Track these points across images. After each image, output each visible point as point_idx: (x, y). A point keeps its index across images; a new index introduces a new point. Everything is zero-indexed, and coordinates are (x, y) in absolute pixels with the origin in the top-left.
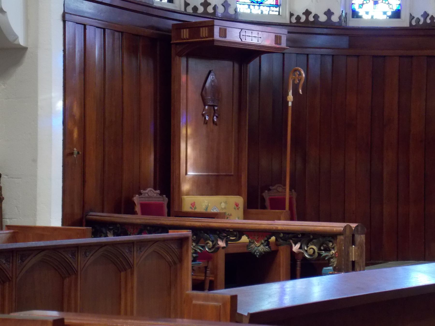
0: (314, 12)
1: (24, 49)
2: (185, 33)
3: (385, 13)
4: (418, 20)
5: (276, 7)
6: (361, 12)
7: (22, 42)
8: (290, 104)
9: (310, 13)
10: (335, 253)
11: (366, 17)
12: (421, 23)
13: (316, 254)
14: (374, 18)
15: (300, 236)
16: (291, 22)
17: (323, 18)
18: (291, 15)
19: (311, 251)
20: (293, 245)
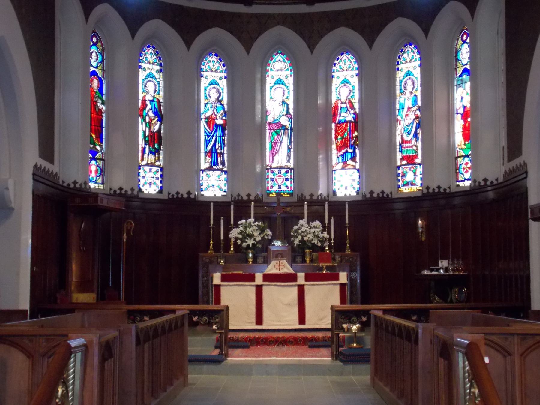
0: (181, 192)
1: (12, 209)
2: (78, 200)
3: (155, 190)
4: (173, 196)
5: (102, 185)
6: (143, 189)
7: (13, 205)
8: (125, 240)
9: (179, 193)
10: (219, 321)
11: (146, 192)
12: (237, 199)
13: (207, 321)
14: (150, 193)
15: (205, 313)
16: (232, 200)
17: (186, 196)
18: (111, 189)
19: (205, 320)
20: (194, 318)
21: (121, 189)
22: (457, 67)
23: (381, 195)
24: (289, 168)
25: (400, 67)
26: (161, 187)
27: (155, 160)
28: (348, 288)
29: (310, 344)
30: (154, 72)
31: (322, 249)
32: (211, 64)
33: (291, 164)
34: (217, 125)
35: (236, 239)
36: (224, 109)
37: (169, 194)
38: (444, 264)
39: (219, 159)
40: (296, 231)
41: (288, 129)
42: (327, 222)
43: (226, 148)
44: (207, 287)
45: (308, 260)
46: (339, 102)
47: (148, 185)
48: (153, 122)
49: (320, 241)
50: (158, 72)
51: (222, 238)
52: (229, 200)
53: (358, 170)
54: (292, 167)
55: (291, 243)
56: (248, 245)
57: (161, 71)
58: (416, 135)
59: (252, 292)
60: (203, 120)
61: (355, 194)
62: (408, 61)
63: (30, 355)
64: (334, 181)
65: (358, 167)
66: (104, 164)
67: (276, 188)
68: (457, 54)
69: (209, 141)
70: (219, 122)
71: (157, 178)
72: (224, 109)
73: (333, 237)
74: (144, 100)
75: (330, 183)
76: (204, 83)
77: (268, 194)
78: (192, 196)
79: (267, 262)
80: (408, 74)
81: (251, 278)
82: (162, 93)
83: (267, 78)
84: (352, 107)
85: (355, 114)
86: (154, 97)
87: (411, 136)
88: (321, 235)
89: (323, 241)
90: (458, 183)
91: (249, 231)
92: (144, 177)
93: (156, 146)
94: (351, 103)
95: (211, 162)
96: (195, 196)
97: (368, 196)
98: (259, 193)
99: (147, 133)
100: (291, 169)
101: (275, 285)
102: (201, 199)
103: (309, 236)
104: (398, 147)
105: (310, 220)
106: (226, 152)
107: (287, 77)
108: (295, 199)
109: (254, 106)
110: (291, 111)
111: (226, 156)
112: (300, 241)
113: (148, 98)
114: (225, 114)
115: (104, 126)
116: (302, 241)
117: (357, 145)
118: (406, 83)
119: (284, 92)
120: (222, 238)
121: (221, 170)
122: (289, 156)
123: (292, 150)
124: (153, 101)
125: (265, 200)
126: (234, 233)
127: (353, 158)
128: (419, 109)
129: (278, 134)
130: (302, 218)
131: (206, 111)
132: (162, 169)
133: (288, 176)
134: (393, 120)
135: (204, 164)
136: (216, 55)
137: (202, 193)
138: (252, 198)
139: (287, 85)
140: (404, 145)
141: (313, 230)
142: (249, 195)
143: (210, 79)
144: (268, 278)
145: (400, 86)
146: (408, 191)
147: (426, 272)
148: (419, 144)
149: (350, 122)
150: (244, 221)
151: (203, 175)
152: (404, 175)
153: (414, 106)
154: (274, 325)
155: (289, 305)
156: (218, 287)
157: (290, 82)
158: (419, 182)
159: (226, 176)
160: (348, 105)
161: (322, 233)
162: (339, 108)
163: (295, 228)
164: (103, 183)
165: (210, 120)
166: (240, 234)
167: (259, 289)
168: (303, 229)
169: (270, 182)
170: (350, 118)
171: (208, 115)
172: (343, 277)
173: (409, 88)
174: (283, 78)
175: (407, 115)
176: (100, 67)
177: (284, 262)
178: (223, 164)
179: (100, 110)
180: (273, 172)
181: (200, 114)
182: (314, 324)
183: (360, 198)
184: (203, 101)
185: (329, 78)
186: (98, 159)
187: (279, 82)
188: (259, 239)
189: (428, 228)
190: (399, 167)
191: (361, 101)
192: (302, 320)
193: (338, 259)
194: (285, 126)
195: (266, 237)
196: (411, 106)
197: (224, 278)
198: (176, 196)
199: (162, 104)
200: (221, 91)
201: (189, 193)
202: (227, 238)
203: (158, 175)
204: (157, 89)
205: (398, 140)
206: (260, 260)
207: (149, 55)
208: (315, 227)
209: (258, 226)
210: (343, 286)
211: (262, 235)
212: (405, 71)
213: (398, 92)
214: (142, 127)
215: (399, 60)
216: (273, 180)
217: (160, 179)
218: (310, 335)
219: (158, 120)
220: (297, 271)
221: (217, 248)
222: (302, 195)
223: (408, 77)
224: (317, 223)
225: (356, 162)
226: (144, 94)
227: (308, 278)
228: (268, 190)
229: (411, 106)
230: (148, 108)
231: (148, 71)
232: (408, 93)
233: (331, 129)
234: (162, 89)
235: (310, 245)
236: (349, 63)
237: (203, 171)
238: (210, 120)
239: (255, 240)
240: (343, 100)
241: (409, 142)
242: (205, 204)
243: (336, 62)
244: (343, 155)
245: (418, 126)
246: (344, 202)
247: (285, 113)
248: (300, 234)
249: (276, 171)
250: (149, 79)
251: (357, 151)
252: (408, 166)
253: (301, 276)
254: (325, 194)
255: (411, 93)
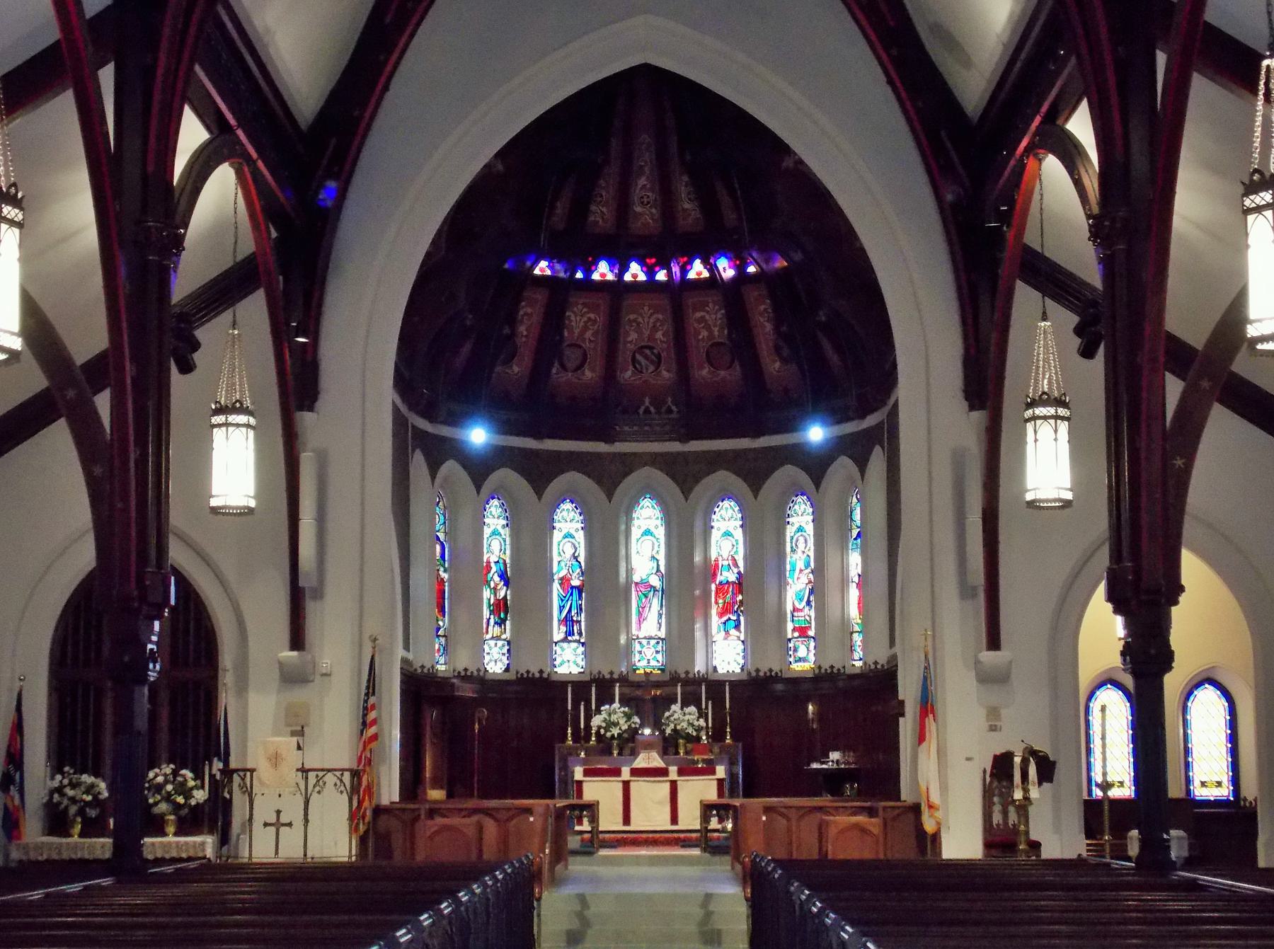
4: (522, 674)
11: (491, 671)
17: (537, 675)
21: (466, 670)
22: (851, 530)
23: (768, 674)
24: (659, 638)
25: (790, 520)
26: (508, 664)
27: (501, 632)
28: (726, 785)
29: (681, 844)
30: (499, 528)
31: (698, 739)
32: (565, 513)
33: (662, 634)
34: (573, 587)
35: (600, 727)
36: (581, 567)
37: (517, 673)
38: (835, 756)
39: (575, 628)
40: (668, 718)
41: (658, 591)
42: (704, 706)
43: (583, 615)
44: (566, 783)
45: (682, 752)
46: (720, 559)
47: (493, 663)
48: (499, 588)
49: (696, 730)
50: (503, 527)
51: (582, 726)
52: (587, 678)
53: (743, 642)
54: (663, 637)
55: (663, 732)
56: (613, 736)
57: (507, 525)
58: (808, 603)
59: (619, 788)
60: (556, 581)
61: (739, 671)
62: (800, 514)
63: (496, 820)
64: (714, 655)
65: (742, 638)
66: (446, 640)
67: (644, 663)
68: (851, 512)
69: (564, 606)
70: (575, 582)
71: (504, 654)
72: (581, 567)
73: (710, 725)
74: (488, 562)
75: (710, 656)
76: (557, 536)
77: (635, 670)
78: (545, 675)
79: (634, 753)
80: (800, 529)
81: (616, 772)
82: (508, 552)
83: (632, 528)
84: (736, 565)
85: (739, 573)
86: (499, 557)
87: (804, 603)
88: (696, 723)
89: (699, 729)
90: (854, 663)
91: (614, 718)
92: (488, 654)
93: (502, 615)
94: (734, 560)
95: (566, 632)
96: (549, 675)
97: (754, 674)
98: (623, 670)
99: (492, 602)
100: (662, 639)
101: (644, 781)
102: (554, 678)
103: (682, 724)
104: (789, 616)
105: (685, 704)
106: (583, 620)
107: (657, 527)
108: (667, 677)
109: (617, 566)
110: (662, 569)
111: (583, 624)
112: (672, 730)
113: (493, 559)
114: (582, 573)
115: (446, 597)
116: (675, 730)
117: (741, 611)
118: (797, 541)
119: (653, 544)
120: (582, 726)
121: (578, 641)
122: (660, 624)
123: (664, 616)
124: (498, 562)
125: (631, 678)
126: (597, 721)
127: (737, 627)
128: (812, 572)
129: (646, 597)
130: (675, 701)
131: (559, 571)
132: (509, 643)
133: (659, 648)
134: (782, 583)
135: (558, 633)
136: (572, 502)
137: (555, 670)
138: (616, 676)
139: (657, 536)
140: (796, 614)
141: (687, 717)
142: (611, 673)
143: (565, 531)
144: (636, 772)
145: (791, 543)
146: (800, 669)
147: (815, 766)
148: (813, 614)
149: (733, 583)
150: (607, 707)
151: (557, 648)
152: (795, 650)
153: (806, 568)
154: (643, 826)
155: (660, 803)
156: (580, 783)
157: (661, 532)
158: (812, 658)
159: (583, 649)
160: (730, 562)
161: (698, 720)
162: (720, 566)
163: (667, 714)
164: (445, 664)
165: (564, 581)
166: (604, 721)
167: (626, 785)
168: (676, 716)
169: (637, 655)
170: (732, 577)
171: (561, 575)
172: (721, 771)
173: (801, 545)
174: (652, 529)
175: (798, 578)
176: (442, 530)
177: (655, 755)
178: (580, 634)
179: (442, 579)
180: (640, 643)
181: (553, 575)
182: (689, 825)
183: (745, 677)
184: (556, 558)
185: (708, 529)
186: (440, 636)
187: (647, 532)
188: (625, 727)
189: (820, 715)
190: (790, 640)
191: (745, 559)
192: (674, 820)
193: (716, 750)
194: (654, 587)
195: (633, 726)
196: (803, 568)
197: (587, 773)
198: (525, 676)
199: (508, 566)
200: (577, 545)
201: (541, 672)
202: (588, 727)
203: (505, 650)
204: (503, 548)
205: (789, 608)
206: (627, 751)
207: (494, 507)
208: (690, 714)
209: (624, 712)
210: (720, 781)
211: (629, 723)
212: (797, 526)
213: (788, 549)
214: (487, 594)
215: (789, 512)
216: (640, 652)
217: (507, 655)
218: (682, 835)
219: (504, 585)
220: (668, 764)
221: (576, 738)
222: (676, 672)
223: (800, 533)
224: (692, 709)
225: (740, 632)
226: (488, 555)
227: (681, 772)
228: (635, 665)
229: (803, 568)
230: (492, 572)
231: (492, 528)
232: (799, 551)
233: (710, 591)
234: (508, 547)
235: (683, 734)
236: (732, 512)
237: (556, 643)
238: (564, 581)
239: (620, 729)
240: (725, 557)
241: (801, 610)
242: (560, 686)
243: (716, 509)
244: (725, 623)
245: (811, 592)
246: (725, 681)
247: (654, 571)
248: (673, 722)
249: (644, 642)
250: (494, 537)
251: (742, 618)
252: (800, 639)
253: (673, 770)
254: (703, 671)
255: (804, 552)
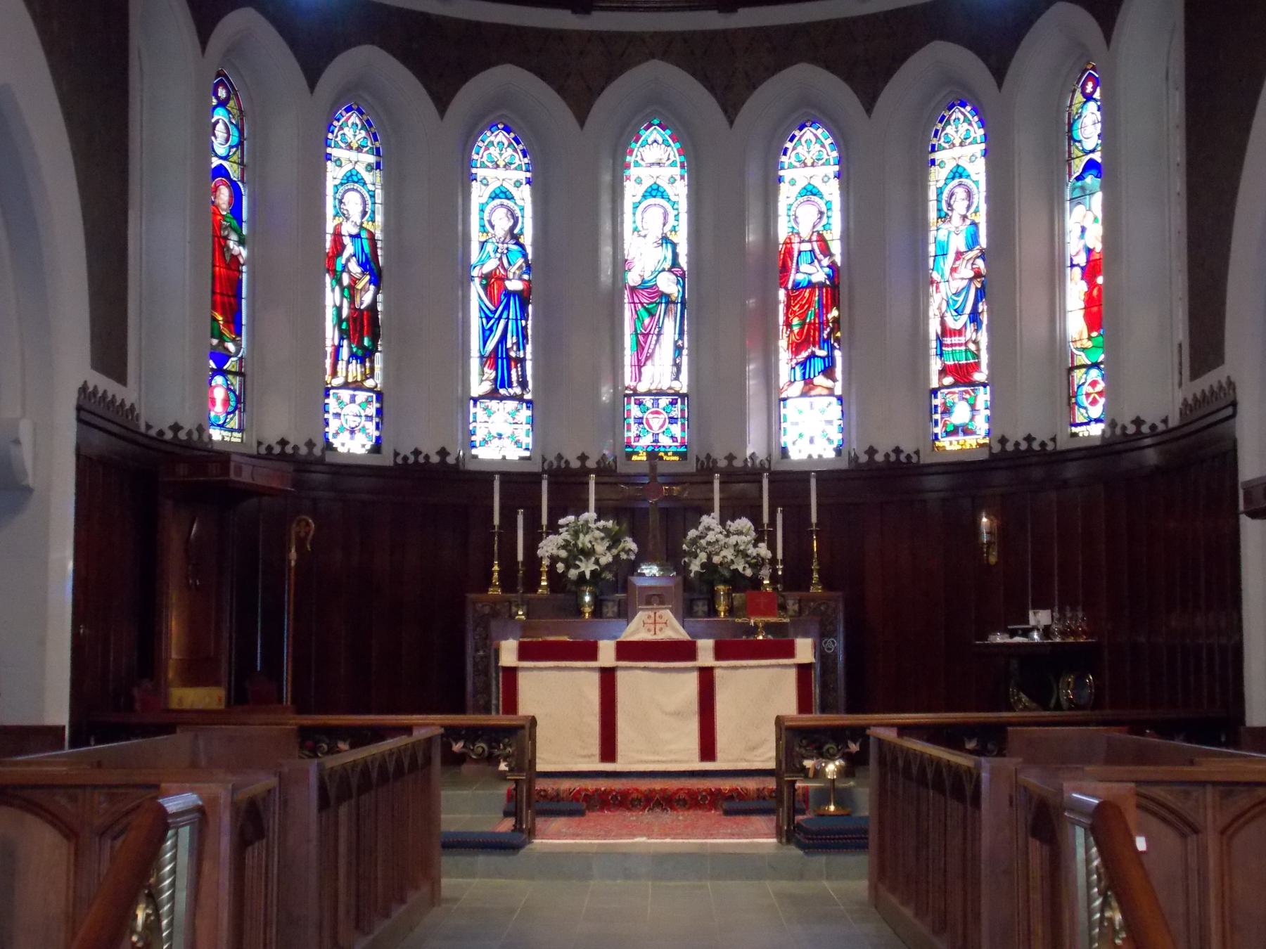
0: (425, 450)
1: (28, 490)
2: (182, 470)
3: (363, 446)
4: (405, 458)
5: (239, 432)
6: (336, 443)
7: (30, 481)
8: (293, 563)
9: (421, 453)
10: (513, 752)
11: (341, 450)
12: (555, 467)
13: (486, 752)
14: (351, 451)
15: (480, 733)
17: (435, 459)
18: (260, 444)
19: (480, 750)
20: (454, 744)
21: (283, 443)
22: (1071, 158)
23: (893, 458)
24: (677, 394)
25: (937, 156)
26: (378, 439)
27: (364, 374)
28: (815, 675)
29: (726, 805)
30: (361, 169)
31: (756, 582)
32: (494, 151)
33: (683, 385)
34: (509, 294)
35: (554, 559)
36: (525, 256)
37: (396, 454)
38: (1040, 618)
39: (513, 372)
40: (694, 541)
41: (675, 303)
42: (766, 519)
43: (529, 348)
44: (486, 673)
45: (722, 608)
46: (796, 239)
47: (347, 434)
48: (359, 286)
49: (751, 565)
50: (370, 168)
51: (520, 557)
52: (536, 468)
53: (840, 398)
54: (684, 390)
55: (683, 570)
56: (582, 575)
57: (378, 165)
58: (975, 317)
59: (590, 685)
60: (477, 281)
61: (831, 454)
62: (957, 142)
63: (69, 832)
64: (783, 425)
65: (838, 391)
66: (243, 385)
67: (647, 440)
68: (1071, 126)
69: (491, 329)
70: (514, 285)
71: (369, 418)
72: (525, 256)
73: (780, 556)
74: (338, 235)
75: (774, 428)
76: (478, 194)
77: (629, 455)
78: (451, 460)
79: (625, 613)
80: (958, 173)
81: (589, 651)
82: (379, 218)
83: (626, 183)
84: (826, 251)
85: (832, 266)
86: (361, 227)
87: (964, 318)
88: (752, 551)
89: (757, 564)
90: (1074, 430)
91: (584, 540)
92: (337, 415)
93: (366, 342)
94: (822, 241)
95: (496, 379)
96: (457, 459)
97: (864, 458)
98: (606, 452)
99: (345, 313)
100: (683, 396)
101: (645, 668)
102: (471, 466)
103: (723, 553)
104: (933, 344)
105: (728, 515)
106: (529, 356)
107: (672, 181)
108: (691, 467)
109: (595, 249)
110: (683, 261)
111: (529, 365)
112: (703, 566)
113: (348, 229)
114: (528, 266)
115: (244, 295)
116: (708, 566)
117: (837, 340)
118: (952, 195)
119: (666, 215)
120: (520, 557)
121: (519, 399)
122: (678, 366)
123: (685, 352)
124: (358, 236)
125: (622, 468)
126: (549, 546)
127: (828, 371)
128: (983, 255)
129: (652, 315)
130: (709, 511)
131: (483, 261)
132: (380, 396)
133: (676, 412)
134: (921, 282)
135: (479, 385)
136: (507, 129)
137: (474, 452)
138: (591, 464)
139: (673, 198)
140: (948, 340)
141: (733, 539)
142: (583, 458)
143: (493, 186)
144: (628, 651)
145: (939, 201)
146: (956, 447)
147: (999, 638)
148: (983, 338)
149: (821, 285)
150: (571, 518)
151: (477, 411)
152: (947, 411)
153: (971, 250)
154: (642, 762)
155: (677, 714)
156: (511, 673)
157: (680, 191)
158: (981, 425)
159: (529, 413)
160: (816, 246)
161: (755, 546)
162: (796, 254)
163: (692, 533)
164: (240, 430)
165: (492, 281)
166: (564, 547)
167: (608, 678)
168: (711, 537)
169: (634, 427)
170: (820, 276)
171: (487, 268)
172: (805, 650)
173: (960, 205)
174: (663, 183)
175: (953, 270)
176: (235, 158)
177: (667, 614)
178: (523, 384)
179: (235, 258)
180: (639, 403)
181: (468, 267)
182: (737, 760)
183: (843, 464)
184: (476, 236)
185: (771, 183)
186: (230, 372)
187: (655, 191)
188: (606, 559)
189: (1003, 534)
190: (934, 392)
191: (845, 237)
192: (708, 749)
193: (792, 606)
194: (668, 296)
195: (624, 556)
196: (963, 249)
197: (526, 652)
198: (412, 459)
199: (379, 245)
200: (518, 213)
201: (443, 453)
202: (532, 558)
203: (372, 410)
204: (369, 210)
205: (934, 327)
206: (610, 609)
207: (350, 129)
208: (739, 533)
209: (604, 529)
210: (803, 670)
211: (615, 551)
212: (950, 165)
213: (933, 215)
214: (332, 297)
215: (934, 141)
216: (639, 421)
217: (376, 420)
218: (726, 785)
219: (370, 282)
220: (695, 635)
221: (508, 582)
222: (708, 456)
223: (956, 181)
224: (744, 523)
225: (834, 380)
226: (337, 221)
227: (722, 652)
228: (629, 445)
229: (963, 249)
230: (346, 254)
231: (347, 167)
232: (956, 219)
233: (777, 302)
234: (379, 208)
235: (727, 574)
236: (818, 147)
237: (475, 400)
238: (492, 281)
239: (597, 562)
240: (805, 235)
241: (959, 333)
242: (481, 479)
243: (789, 145)
244: (803, 364)
245: (981, 294)
246: (807, 473)
247: (667, 265)
248: (703, 549)
249: (648, 401)
250: (350, 186)
251: (838, 354)
252: (956, 390)
253: (706, 646)
254: (762, 455)
255: (964, 217)
